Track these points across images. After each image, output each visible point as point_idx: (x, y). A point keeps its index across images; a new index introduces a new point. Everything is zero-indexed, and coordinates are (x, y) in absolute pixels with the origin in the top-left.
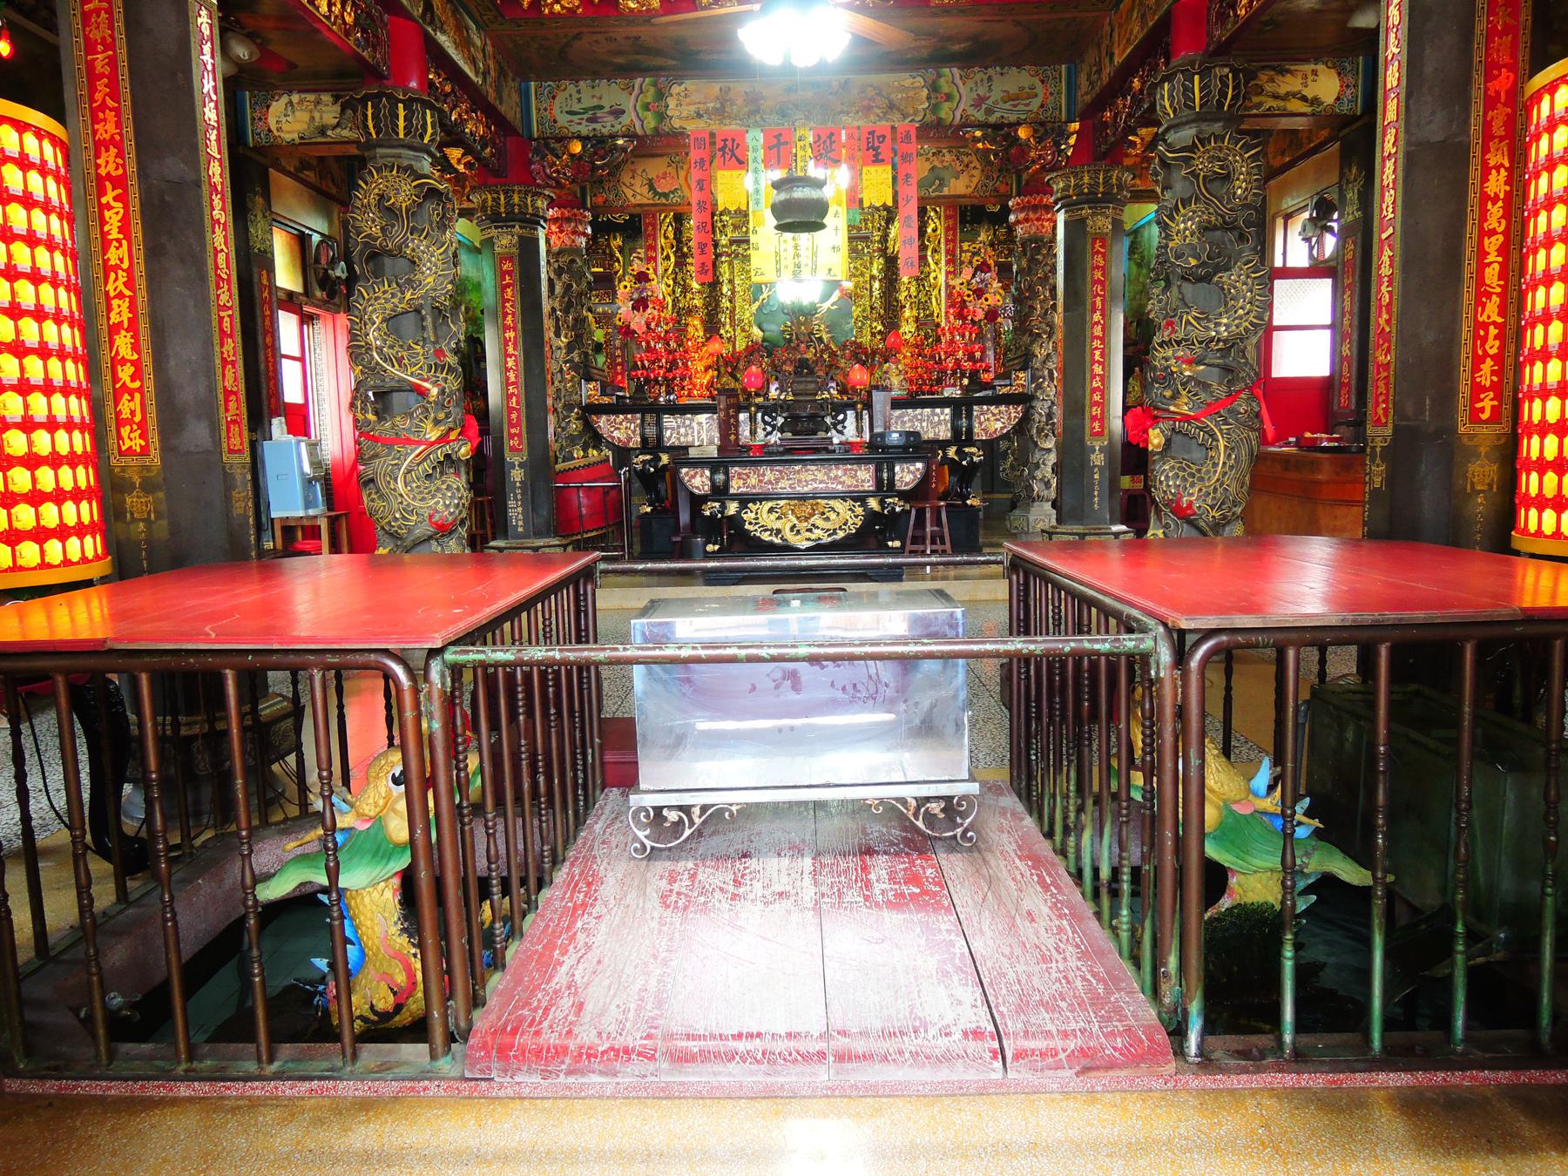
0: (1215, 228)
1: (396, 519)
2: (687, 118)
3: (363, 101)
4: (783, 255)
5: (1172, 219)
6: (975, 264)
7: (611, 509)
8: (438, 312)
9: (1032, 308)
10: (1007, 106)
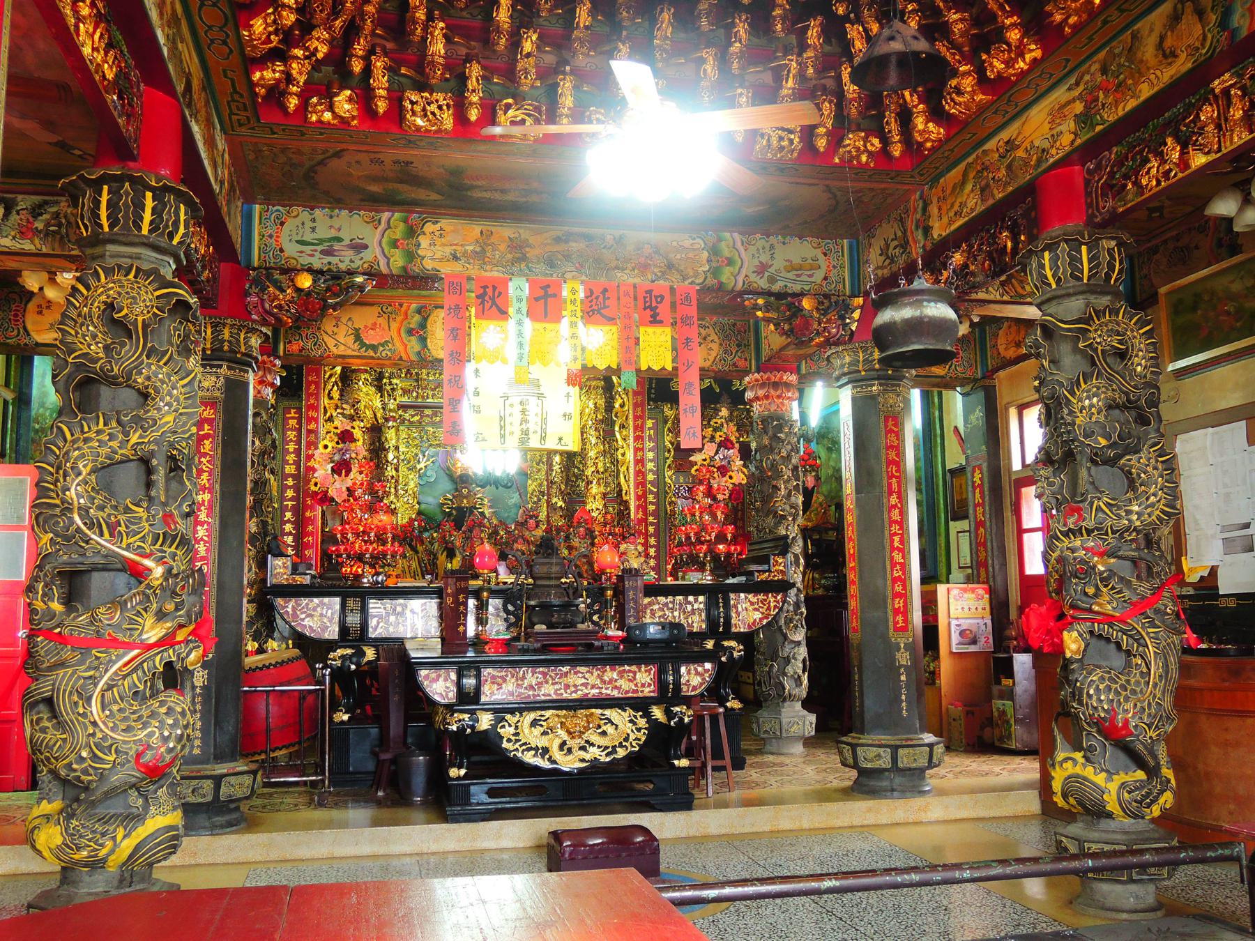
0: (1117, 406)
1: (82, 759)
2: (441, 260)
3: (97, 185)
4: (508, 420)
5: (1073, 394)
6: (718, 439)
7: (306, 722)
8: (174, 466)
9: (777, 488)
10: (790, 275)
